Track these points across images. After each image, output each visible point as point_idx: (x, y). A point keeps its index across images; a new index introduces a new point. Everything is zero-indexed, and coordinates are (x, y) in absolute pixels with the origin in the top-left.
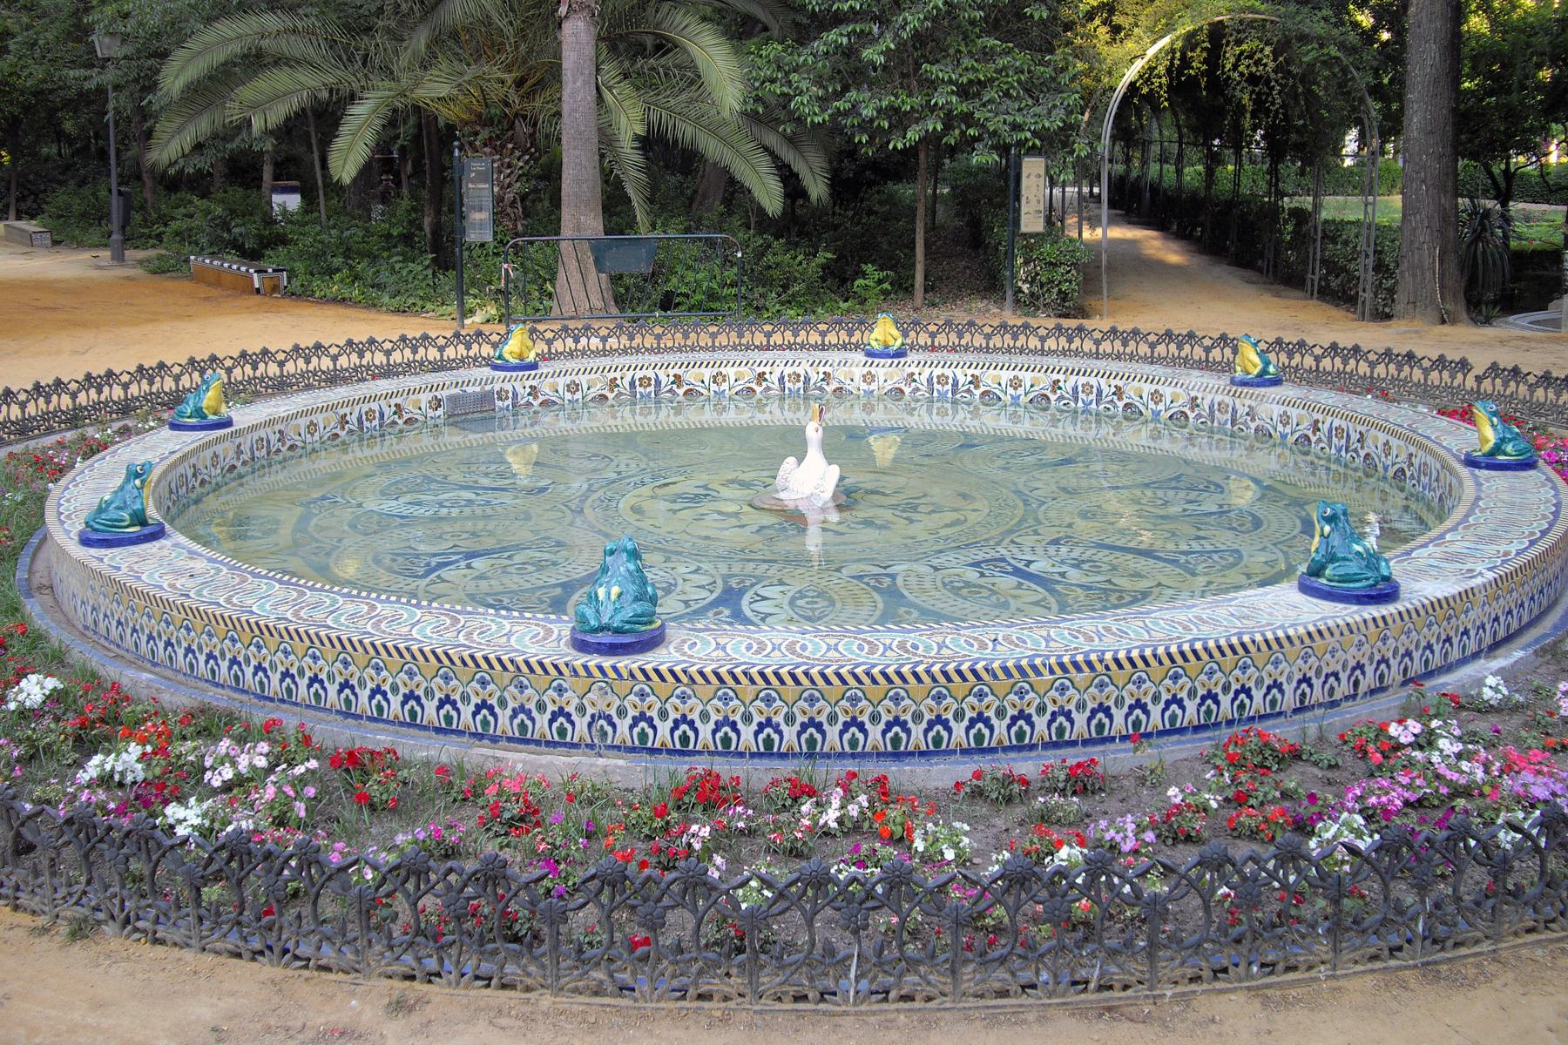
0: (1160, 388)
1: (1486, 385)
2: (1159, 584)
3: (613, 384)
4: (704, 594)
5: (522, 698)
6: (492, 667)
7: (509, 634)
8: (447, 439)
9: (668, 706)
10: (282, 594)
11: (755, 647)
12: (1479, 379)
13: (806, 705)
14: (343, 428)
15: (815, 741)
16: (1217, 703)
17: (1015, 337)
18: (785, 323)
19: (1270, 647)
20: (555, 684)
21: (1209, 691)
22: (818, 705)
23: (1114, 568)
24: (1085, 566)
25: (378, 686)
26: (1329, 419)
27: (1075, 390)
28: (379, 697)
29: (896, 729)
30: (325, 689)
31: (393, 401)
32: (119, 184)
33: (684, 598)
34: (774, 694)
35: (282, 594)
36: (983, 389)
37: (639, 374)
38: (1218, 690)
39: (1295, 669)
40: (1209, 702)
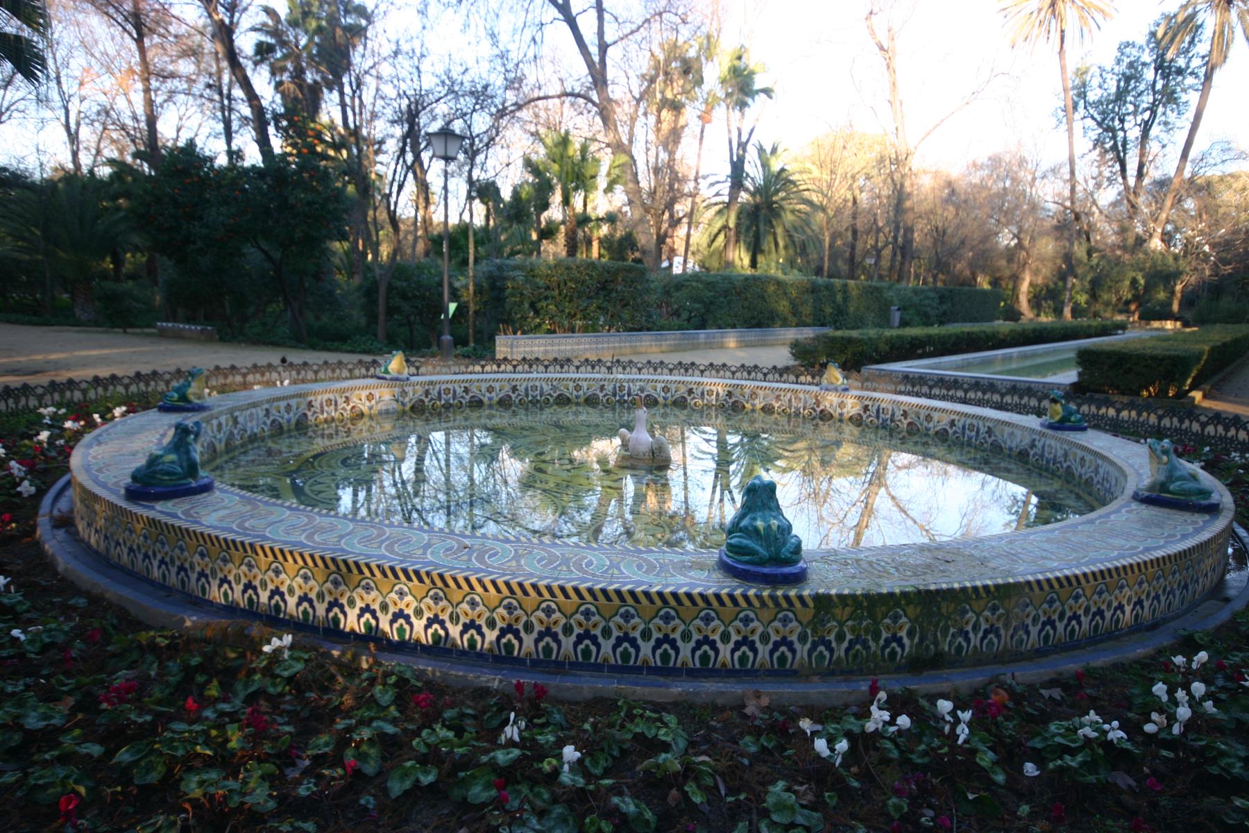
6: (446, 585)
8: (583, 417)
9: (611, 624)
13: (621, 621)
15: (551, 650)
22: (713, 624)
28: (277, 597)
29: (548, 639)
30: (231, 588)
32: (502, 257)
34: (713, 614)
39: (1040, 612)
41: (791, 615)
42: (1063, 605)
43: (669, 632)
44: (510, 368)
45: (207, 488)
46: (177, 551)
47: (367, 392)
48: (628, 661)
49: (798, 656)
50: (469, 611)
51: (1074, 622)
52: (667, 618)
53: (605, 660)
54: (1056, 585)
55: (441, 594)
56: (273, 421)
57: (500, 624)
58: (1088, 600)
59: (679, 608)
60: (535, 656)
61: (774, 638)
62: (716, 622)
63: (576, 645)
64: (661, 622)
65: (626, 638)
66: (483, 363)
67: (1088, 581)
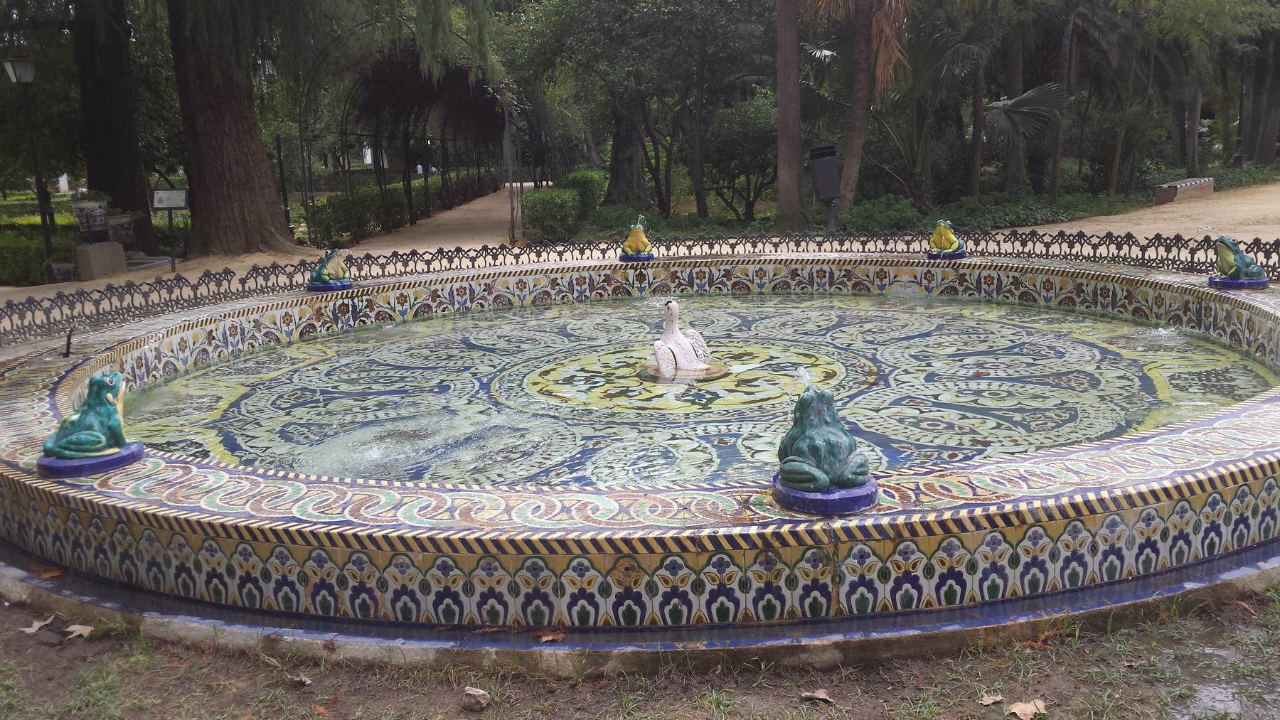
0: (885, 269)
1: (251, 284)
3: (435, 295)
12: (243, 281)
14: (210, 344)
15: (542, 613)
16: (1156, 551)
18: (921, 233)
19: (1203, 490)
20: (528, 563)
21: (1148, 539)
22: (681, 573)
23: (916, 425)
24: (924, 425)
25: (248, 574)
26: (1093, 283)
27: (571, 283)
28: (215, 581)
31: (252, 317)
36: (734, 280)
37: (456, 286)
38: (1156, 537)
39: (1259, 501)
40: (1148, 550)
42: (1094, 536)
43: (585, 586)
44: (421, 266)
47: (283, 312)
48: (634, 622)
50: (486, 578)
51: (1242, 526)
52: (674, 568)
54: (1187, 493)
57: (524, 590)
58: (1228, 506)
59: (734, 553)
61: (939, 570)
62: (546, 573)
63: (480, 605)
64: (667, 573)
65: (674, 592)
66: (732, 241)
67: (1225, 485)
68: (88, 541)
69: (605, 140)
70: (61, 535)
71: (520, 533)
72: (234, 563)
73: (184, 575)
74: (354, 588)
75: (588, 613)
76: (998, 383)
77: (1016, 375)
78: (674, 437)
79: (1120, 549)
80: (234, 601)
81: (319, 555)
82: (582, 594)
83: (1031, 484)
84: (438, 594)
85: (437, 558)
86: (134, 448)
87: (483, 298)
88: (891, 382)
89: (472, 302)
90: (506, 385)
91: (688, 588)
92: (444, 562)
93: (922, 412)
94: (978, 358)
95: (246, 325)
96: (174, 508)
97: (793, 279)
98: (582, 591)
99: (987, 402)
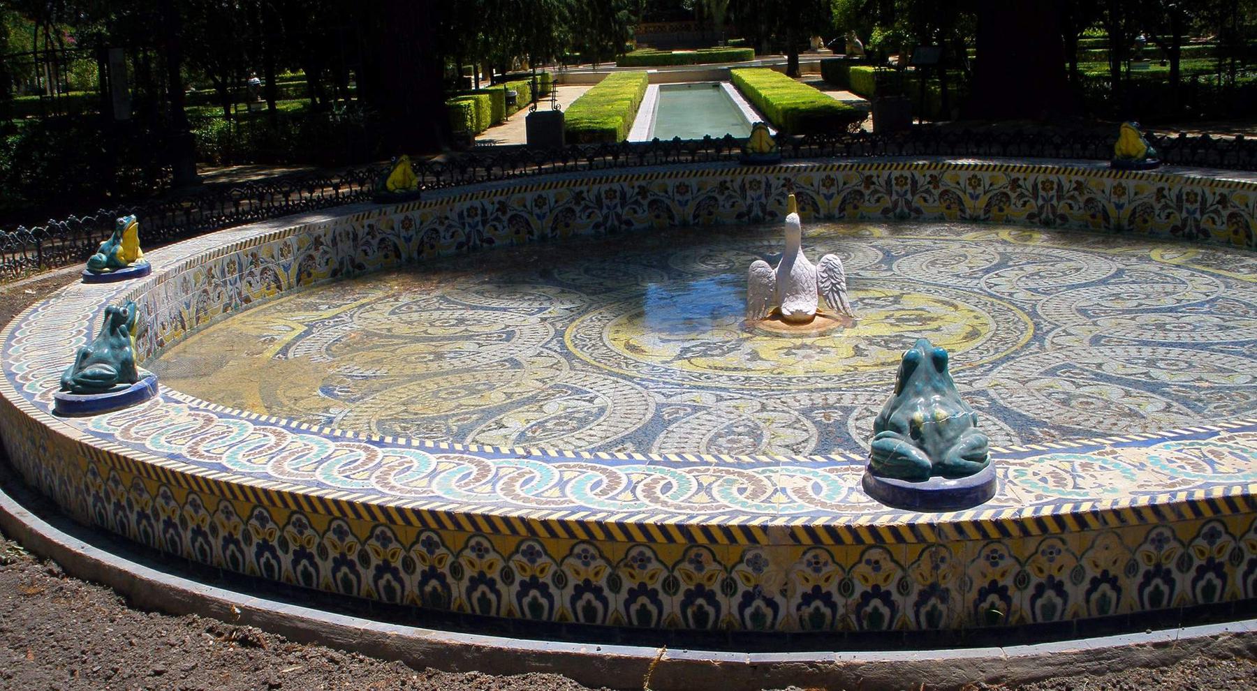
0: (544, 194)
2: (1024, 383)
4: (539, 384)
5: (482, 564)
7: (562, 484)
10: (256, 439)
11: (750, 488)
15: (594, 610)
17: (463, 171)
23: (1065, 402)
28: (345, 569)
33: (503, 431)
35: (256, 439)
36: (650, 198)
41: (592, 550)
45: (139, 396)
46: (160, 501)
47: (535, 194)
49: (1071, 602)
53: (563, 617)
55: (436, 538)
56: (1089, 201)
59: (712, 547)
60: (682, 625)
63: (574, 600)
68: (155, 510)
69: (108, 30)
70: (102, 495)
71: (573, 513)
72: (326, 543)
73: (267, 554)
74: (335, 560)
75: (707, 614)
76: (1178, 350)
77: (1202, 340)
78: (764, 408)
79: (1221, 565)
80: (510, 612)
81: (299, 520)
82: (700, 591)
83: (1079, 480)
84: (472, 579)
85: (421, 532)
86: (142, 383)
87: (927, 191)
88: (1047, 344)
89: (913, 194)
90: (1013, 337)
91: (658, 586)
92: (428, 537)
93: (1078, 386)
94: (1154, 316)
95: (489, 207)
96: (194, 463)
97: (1013, 190)
98: (700, 587)
99: (1161, 375)
